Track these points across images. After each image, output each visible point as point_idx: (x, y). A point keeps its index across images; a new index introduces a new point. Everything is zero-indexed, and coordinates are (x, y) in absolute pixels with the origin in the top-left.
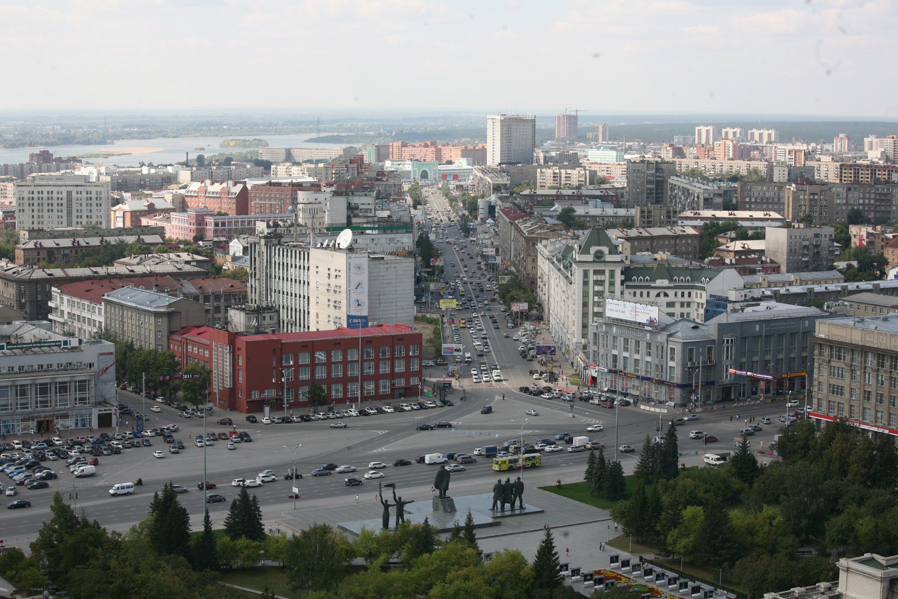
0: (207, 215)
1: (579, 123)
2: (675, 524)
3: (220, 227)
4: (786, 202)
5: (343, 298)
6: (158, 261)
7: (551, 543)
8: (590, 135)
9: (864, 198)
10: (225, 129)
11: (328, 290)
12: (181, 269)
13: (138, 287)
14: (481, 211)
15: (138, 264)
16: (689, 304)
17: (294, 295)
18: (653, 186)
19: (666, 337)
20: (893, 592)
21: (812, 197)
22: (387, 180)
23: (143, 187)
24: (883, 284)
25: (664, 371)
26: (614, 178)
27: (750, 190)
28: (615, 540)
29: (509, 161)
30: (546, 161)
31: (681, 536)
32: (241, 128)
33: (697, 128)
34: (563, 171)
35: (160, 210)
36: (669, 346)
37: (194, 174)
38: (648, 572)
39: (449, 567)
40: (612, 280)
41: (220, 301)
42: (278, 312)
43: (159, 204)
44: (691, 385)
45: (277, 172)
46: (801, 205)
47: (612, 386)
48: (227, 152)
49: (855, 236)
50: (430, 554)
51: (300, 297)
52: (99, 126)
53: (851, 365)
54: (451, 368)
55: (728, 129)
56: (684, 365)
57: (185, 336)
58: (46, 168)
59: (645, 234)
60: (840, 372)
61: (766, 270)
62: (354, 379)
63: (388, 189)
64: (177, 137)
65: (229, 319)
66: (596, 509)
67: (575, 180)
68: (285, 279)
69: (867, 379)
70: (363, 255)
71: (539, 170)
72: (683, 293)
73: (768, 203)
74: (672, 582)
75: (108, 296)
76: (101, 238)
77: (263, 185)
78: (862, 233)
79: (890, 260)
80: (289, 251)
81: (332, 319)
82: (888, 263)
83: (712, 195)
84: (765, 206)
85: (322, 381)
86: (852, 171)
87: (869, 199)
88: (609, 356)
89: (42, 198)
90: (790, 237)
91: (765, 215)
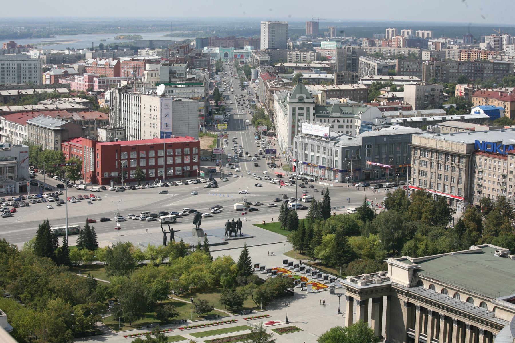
0: (94, 77)
1: (320, 26)
2: (319, 243)
3: (102, 84)
4: (423, 71)
5: (158, 122)
6: (61, 102)
7: (247, 252)
8: (325, 33)
9: (468, 69)
10: (118, 29)
11: (150, 118)
12: (74, 107)
13: (46, 116)
14: (253, 75)
15: (51, 104)
16: (351, 127)
17: (133, 121)
18: (350, 62)
19: (333, 144)
20: (415, 276)
21: (437, 68)
22: (201, 58)
23: (65, 62)
24: (467, 117)
25: (332, 163)
26: (331, 57)
27: (403, 64)
28: (288, 252)
29: (273, 47)
30: (294, 48)
31: (321, 250)
32: (128, 29)
33: (387, 30)
34: (302, 53)
35: (71, 74)
36: (335, 149)
37: (94, 55)
38: (302, 269)
39: (192, 264)
40: (293, 113)
41: (93, 124)
42: (125, 130)
43: (70, 71)
44: (347, 171)
45: (141, 53)
46: (431, 73)
47: (305, 172)
48: (118, 42)
49: (457, 90)
50: (183, 258)
51: (136, 122)
52: (47, 28)
53: (431, 160)
54: (218, 161)
55: (389, 29)
56: (343, 159)
57: (70, 143)
58: (12, 51)
59: (336, 88)
60: (425, 164)
61: (403, 109)
62: (161, 166)
63: (201, 63)
64: (91, 33)
65: (98, 134)
66: (282, 236)
67: (309, 58)
68: (129, 112)
69: (440, 167)
70: (169, 98)
71: (288, 53)
72: (348, 120)
73: (413, 72)
74: (314, 274)
75: (30, 121)
76: (34, 90)
77: (129, 61)
78: (461, 89)
79: (475, 104)
80: (131, 96)
81: (152, 134)
82: (473, 105)
83: (382, 67)
84: (411, 73)
85: (143, 168)
86: (467, 54)
87: (471, 70)
88: (303, 155)
89: (4, 68)
90: (417, 90)
91: (410, 78)
